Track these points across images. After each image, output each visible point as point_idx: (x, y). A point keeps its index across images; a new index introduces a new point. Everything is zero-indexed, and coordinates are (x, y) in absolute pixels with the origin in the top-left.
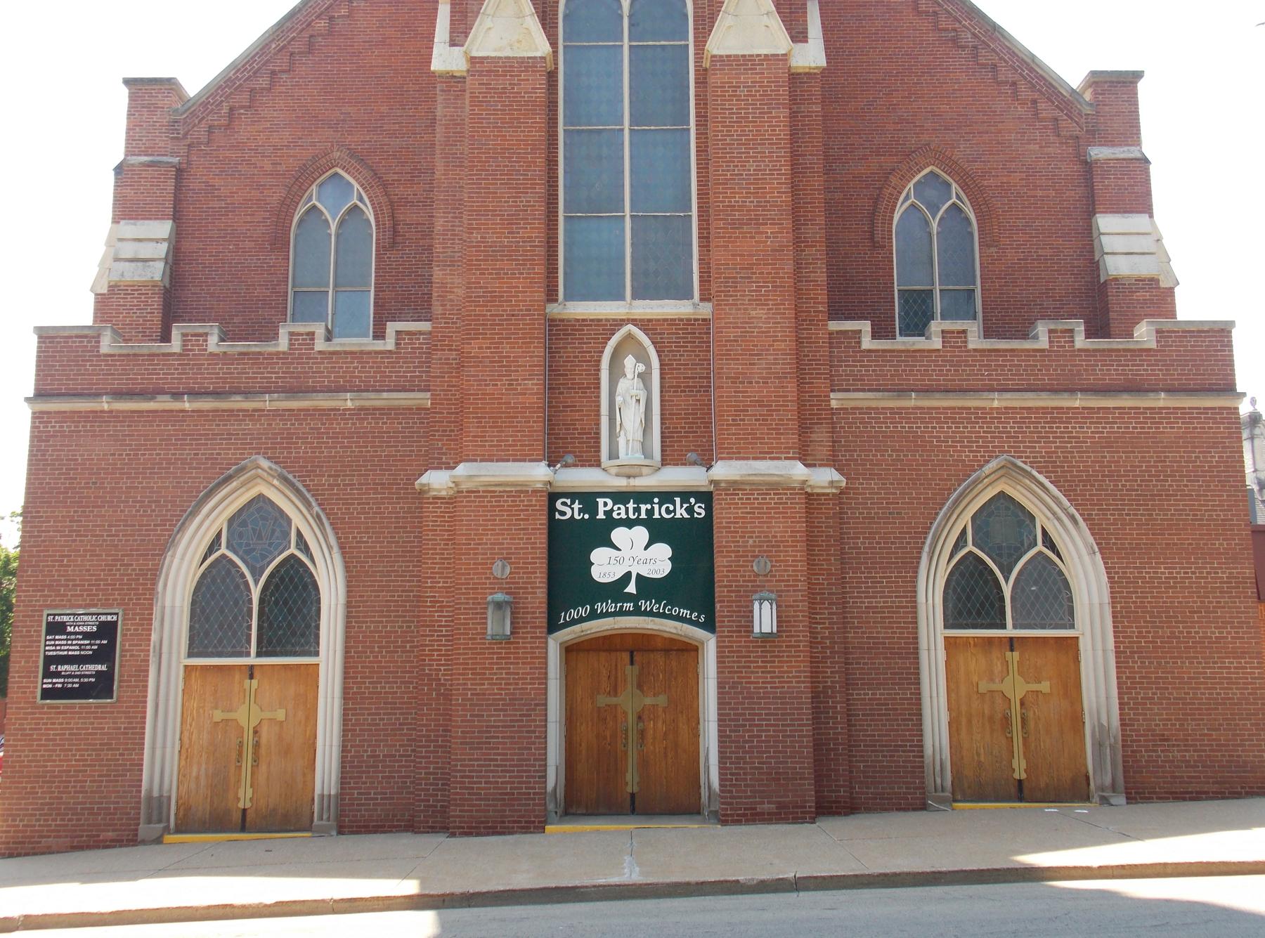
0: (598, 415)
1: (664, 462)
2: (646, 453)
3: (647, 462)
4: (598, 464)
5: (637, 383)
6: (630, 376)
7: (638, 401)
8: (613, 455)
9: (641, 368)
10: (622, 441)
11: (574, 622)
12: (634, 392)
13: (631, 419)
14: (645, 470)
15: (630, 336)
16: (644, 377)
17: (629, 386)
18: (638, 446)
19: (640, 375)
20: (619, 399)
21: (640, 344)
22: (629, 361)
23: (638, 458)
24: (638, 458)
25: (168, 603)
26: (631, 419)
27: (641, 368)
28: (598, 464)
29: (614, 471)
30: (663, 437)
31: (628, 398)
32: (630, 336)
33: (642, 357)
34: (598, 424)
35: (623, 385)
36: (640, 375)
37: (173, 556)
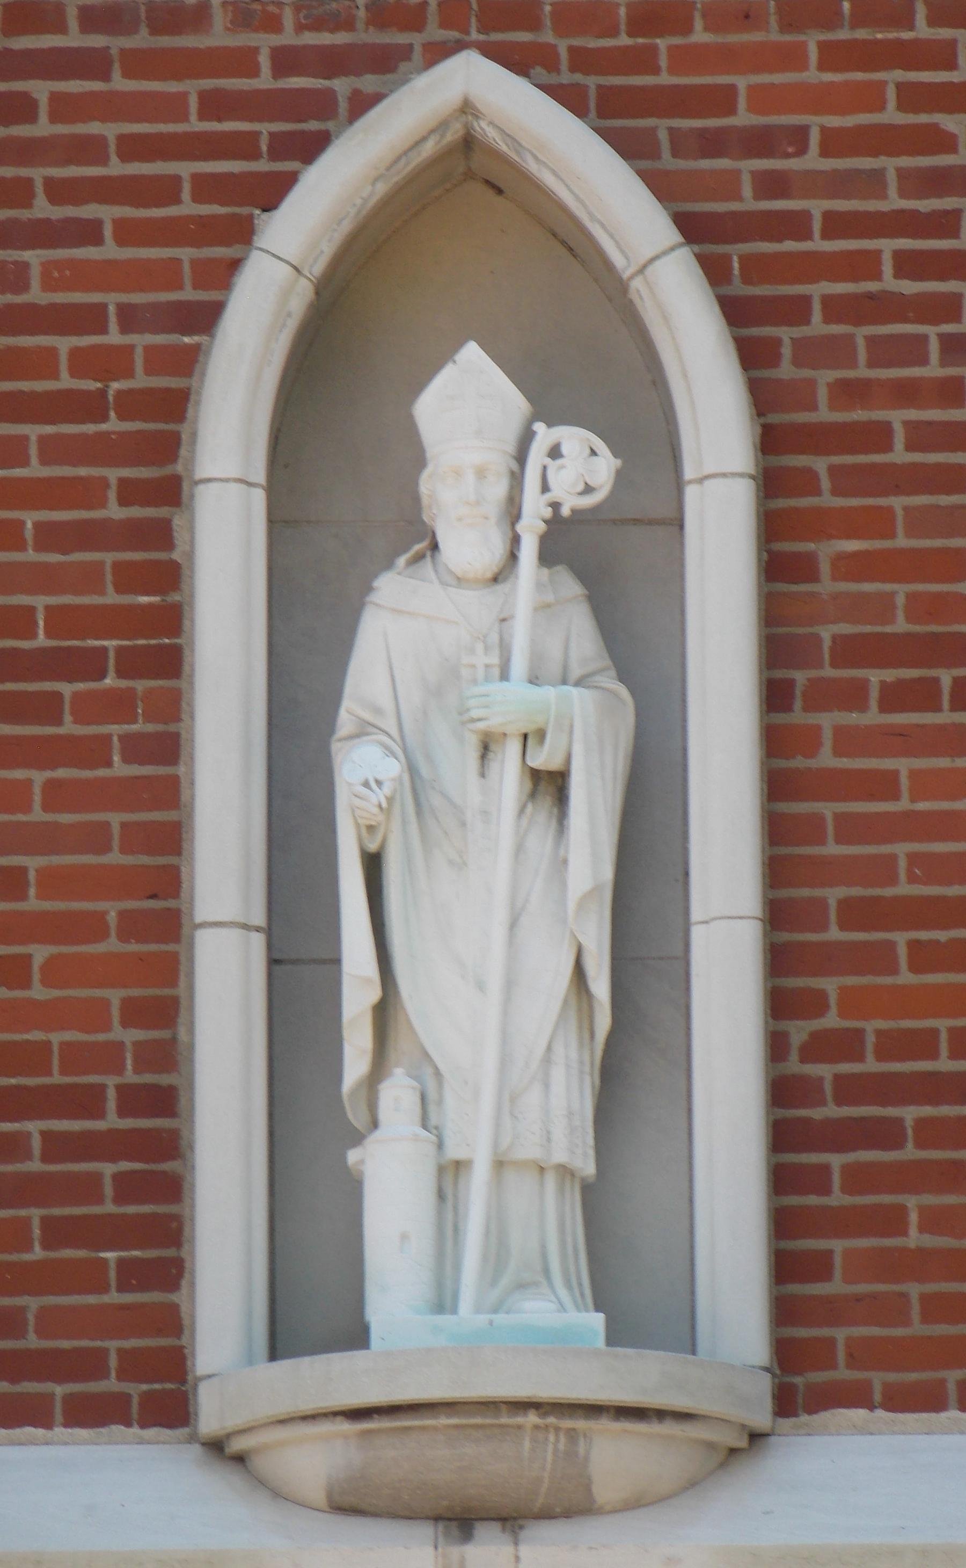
0: (162, 920)
1: (810, 1374)
2: (629, 1278)
3: (640, 1376)
4: (159, 1396)
5: (542, 613)
6: (468, 542)
7: (550, 786)
8: (313, 1305)
9: (580, 467)
10: (391, 1178)
11: (519, 849)
12: (510, 702)
13: (483, 961)
14: (614, 1457)
15: (467, 165)
16: (611, 560)
17: (459, 648)
18: (547, 1222)
19: (569, 542)
20: (362, 771)
21: (568, 241)
22: (465, 410)
23: (546, 1334)
24: (546, 1334)
25: (588, 1079)
26: (483, 961)
27: (580, 467)
28: (159, 1396)
29: (314, 1461)
30: (790, 1134)
31: (454, 764)
32: (467, 165)
33: (588, 367)
34: (163, 1011)
35: (402, 635)
36: (569, 542)
37: (593, 1087)
